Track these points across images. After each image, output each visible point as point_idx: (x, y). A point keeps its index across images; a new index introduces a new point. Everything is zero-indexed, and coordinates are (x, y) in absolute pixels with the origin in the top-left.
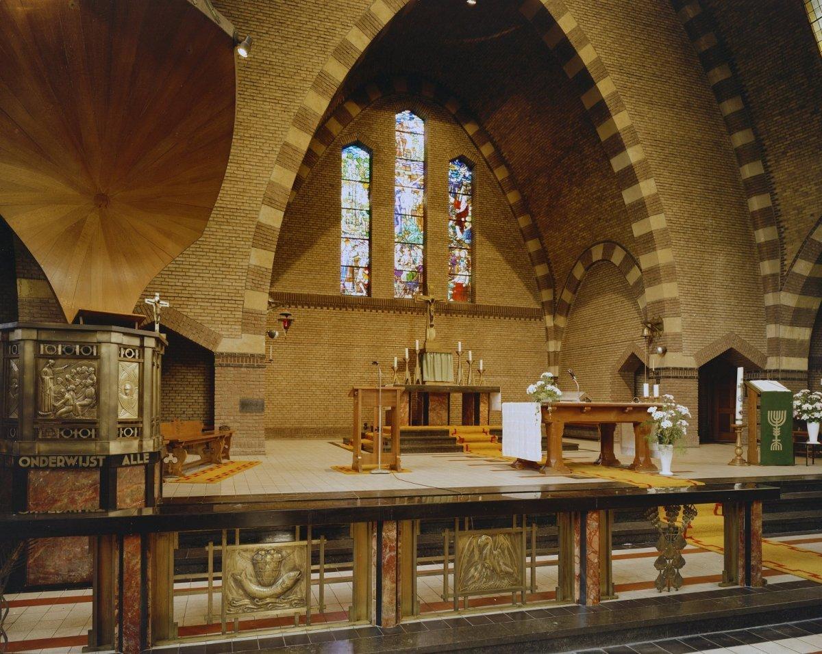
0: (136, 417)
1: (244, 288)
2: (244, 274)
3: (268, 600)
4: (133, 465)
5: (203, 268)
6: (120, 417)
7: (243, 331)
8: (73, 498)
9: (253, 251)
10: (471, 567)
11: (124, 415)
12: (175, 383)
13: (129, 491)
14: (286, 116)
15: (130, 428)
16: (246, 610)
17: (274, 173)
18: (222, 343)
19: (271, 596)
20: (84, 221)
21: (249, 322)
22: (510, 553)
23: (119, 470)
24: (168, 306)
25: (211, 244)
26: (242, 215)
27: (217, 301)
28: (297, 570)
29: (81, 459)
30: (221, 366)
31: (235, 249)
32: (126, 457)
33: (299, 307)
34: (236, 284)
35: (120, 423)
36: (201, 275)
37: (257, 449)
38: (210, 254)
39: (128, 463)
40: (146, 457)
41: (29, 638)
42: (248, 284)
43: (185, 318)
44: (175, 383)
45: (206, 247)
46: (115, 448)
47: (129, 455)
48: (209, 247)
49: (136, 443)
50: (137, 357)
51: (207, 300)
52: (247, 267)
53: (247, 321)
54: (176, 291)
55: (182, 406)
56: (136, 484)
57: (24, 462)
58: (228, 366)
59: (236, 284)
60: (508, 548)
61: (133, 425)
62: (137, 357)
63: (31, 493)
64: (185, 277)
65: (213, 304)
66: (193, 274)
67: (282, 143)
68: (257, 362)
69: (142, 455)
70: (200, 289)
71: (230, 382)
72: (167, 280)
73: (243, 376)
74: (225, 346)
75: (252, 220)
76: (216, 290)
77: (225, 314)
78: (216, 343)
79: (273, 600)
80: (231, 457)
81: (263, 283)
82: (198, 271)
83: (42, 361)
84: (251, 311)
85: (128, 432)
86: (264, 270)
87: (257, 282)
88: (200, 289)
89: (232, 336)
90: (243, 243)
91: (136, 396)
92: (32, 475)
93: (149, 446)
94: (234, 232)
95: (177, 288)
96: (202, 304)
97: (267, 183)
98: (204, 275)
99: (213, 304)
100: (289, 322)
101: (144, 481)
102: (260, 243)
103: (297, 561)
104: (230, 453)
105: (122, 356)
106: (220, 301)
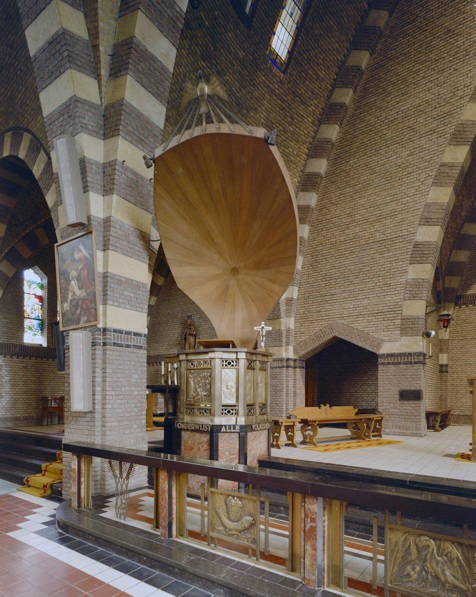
0: (235, 403)
1: (402, 300)
2: (402, 288)
3: (233, 532)
4: (228, 432)
5: (369, 291)
6: (223, 403)
7: (402, 334)
8: (199, 448)
9: (411, 268)
10: (407, 564)
11: (226, 401)
12: (367, 378)
13: (228, 448)
14: (442, 140)
15: (229, 409)
16: (219, 532)
17: (430, 195)
18: (384, 346)
19: (236, 530)
20: (228, 286)
21: (407, 327)
22: (461, 566)
23: (219, 434)
24: (271, 329)
25: (375, 271)
26: (401, 240)
27: (379, 314)
28: (252, 517)
29: (201, 426)
30: (383, 364)
31: (395, 270)
32: (224, 427)
33: (464, 307)
34: (395, 298)
35: (223, 406)
36: (367, 296)
37: (414, 432)
38: (375, 279)
39: (225, 430)
40: (237, 428)
41: (275, 536)
42: (406, 295)
43: (356, 331)
44: (367, 378)
45: (371, 274)
46: (218, 420)
47: (225, 426)
48: (373, 274)
49: (234, 418)
50: (234, 366)
51: (372, 315)
52: (405, 282)
53: (404, 326)
54: (349, 312)
55: (372, 396)
56: (232, 444)
57: (180, 425)
58: (389, 363)
59: (395, 298)
60: (458, 560)
61: (232, 408)
62: (234, 366)
63: (183, 442)
64: (356, 301)
65: (377, 317)
66: (362, 297)
67: (438, 166)
68: (414, 359)
69: (234, 426)
70: (367, 307)
71: (390, 377)
72: (343, 305)
73: (402, 371)
74: (386, 349)
75: (409, 242)
76: (379, 306)
77: (386, 323)
78: (379, 346)
79: (237, 533)
80: (383, 436)
81: (419, 292)
82: (365, 294)
83: (189, 371)
84: (408, 318)
85: (229, 412)
86: (419, 281)
87: (414, 292)
88: (367, 307)
89: (391, 340)
90: (401, 263)
91: (234, 390)
92: (184, 434)
93: (242, 421)
94: (394, 256)
95: (350, 309)
96: (368, 318)
97: (423, 206)
98: (370, 296)
99: (377, 317)
100: (448, 321)
101: (238, 443)
102: (417, 259)
103: (252, 511)
104: (382, 433)
105: (224, 365)
106: (382, 314)
